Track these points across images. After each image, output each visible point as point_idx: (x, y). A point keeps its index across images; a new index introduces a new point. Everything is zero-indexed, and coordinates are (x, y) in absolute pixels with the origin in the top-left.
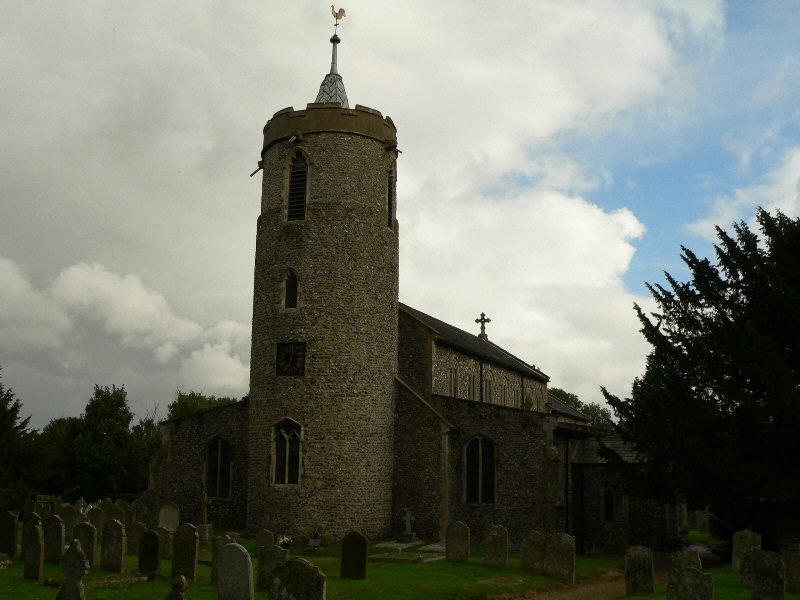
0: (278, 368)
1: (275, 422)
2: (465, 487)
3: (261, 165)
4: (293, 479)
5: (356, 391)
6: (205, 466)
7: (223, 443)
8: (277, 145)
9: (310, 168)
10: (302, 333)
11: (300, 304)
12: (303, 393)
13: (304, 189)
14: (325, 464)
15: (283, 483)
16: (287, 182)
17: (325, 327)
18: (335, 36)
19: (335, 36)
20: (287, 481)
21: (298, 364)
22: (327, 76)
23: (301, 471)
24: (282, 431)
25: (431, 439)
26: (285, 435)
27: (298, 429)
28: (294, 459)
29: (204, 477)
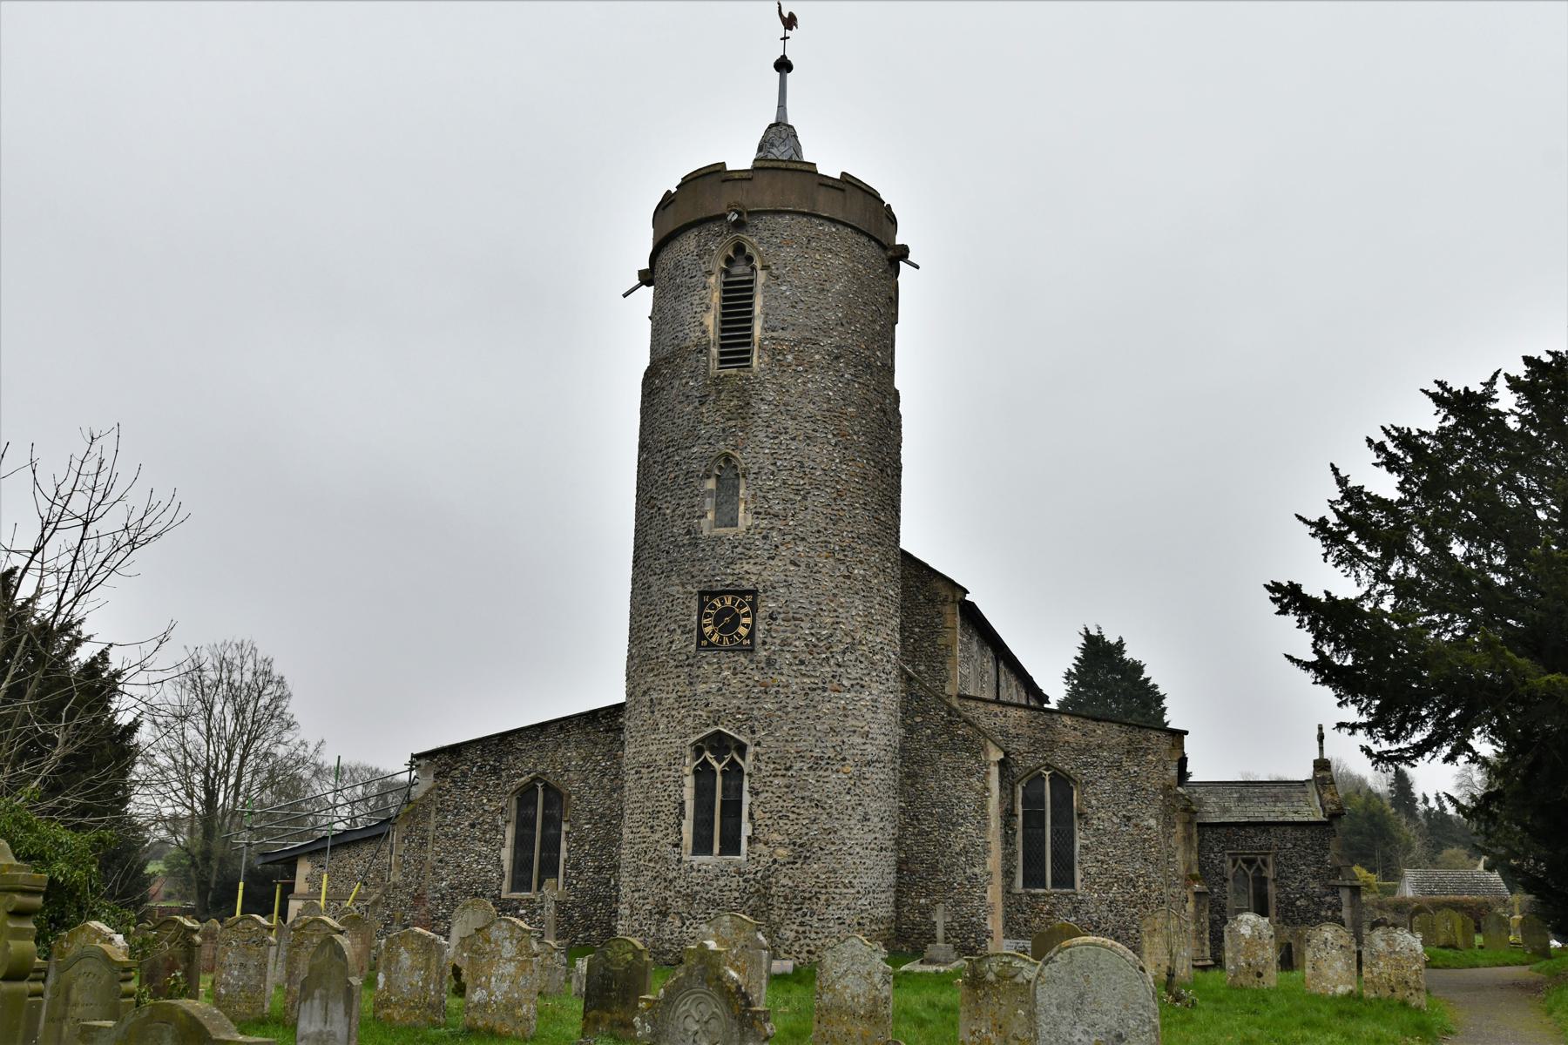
1: (693, 739)
3: (646, 278)
5: (845, 682)
6: (510, 832)
8: (693, 234)
9: (761, 277)
10: (750, 573)
12: (751, 683)
14: (792, 816)
15: (709, 851)
16: (715, 298)
17: (793, 563)
18: (784, 57)
19: (784, 57)
21: (743, 631)
22: (771, 126)
23: (746, 829)
24: (707, 754)
25: (969, 773)
26: (715, 763)
27: (741, 749)
28: (732, 808)
29: (506, 854)
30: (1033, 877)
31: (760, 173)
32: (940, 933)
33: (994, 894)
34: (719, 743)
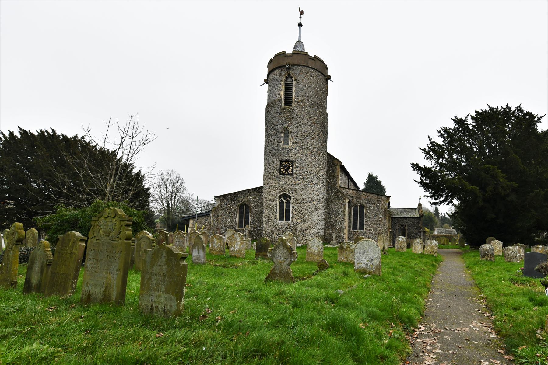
0: (281, 171)
1: (279, 195)
2: (352, 224)
4: (288, 219)
5: (314, 183)
6: (238, 215)
7: (246, 205)
9: (294, 82)
10: (292, 156)
11: (291, 144)
12: (292, 182)
13: (292, 92)
14: (301, 213)
15: (283, 220)
18: (300, 23)
19: (300, 23)
20: (284, 219)
21: (290, 170)
23: (291, 215)
24: (282, 198)
25: (341, 204)
26: (284, 200)
27: (290, 197)
28: (288, 211)
29: (237, 220)
30: (355, 227)
31: (294, 55)
32: (334, 239)
33: (346, 231)
34: (285, 196)
